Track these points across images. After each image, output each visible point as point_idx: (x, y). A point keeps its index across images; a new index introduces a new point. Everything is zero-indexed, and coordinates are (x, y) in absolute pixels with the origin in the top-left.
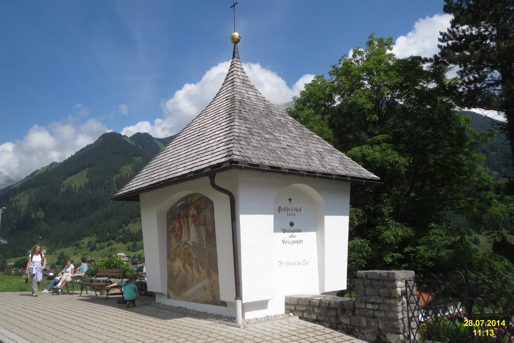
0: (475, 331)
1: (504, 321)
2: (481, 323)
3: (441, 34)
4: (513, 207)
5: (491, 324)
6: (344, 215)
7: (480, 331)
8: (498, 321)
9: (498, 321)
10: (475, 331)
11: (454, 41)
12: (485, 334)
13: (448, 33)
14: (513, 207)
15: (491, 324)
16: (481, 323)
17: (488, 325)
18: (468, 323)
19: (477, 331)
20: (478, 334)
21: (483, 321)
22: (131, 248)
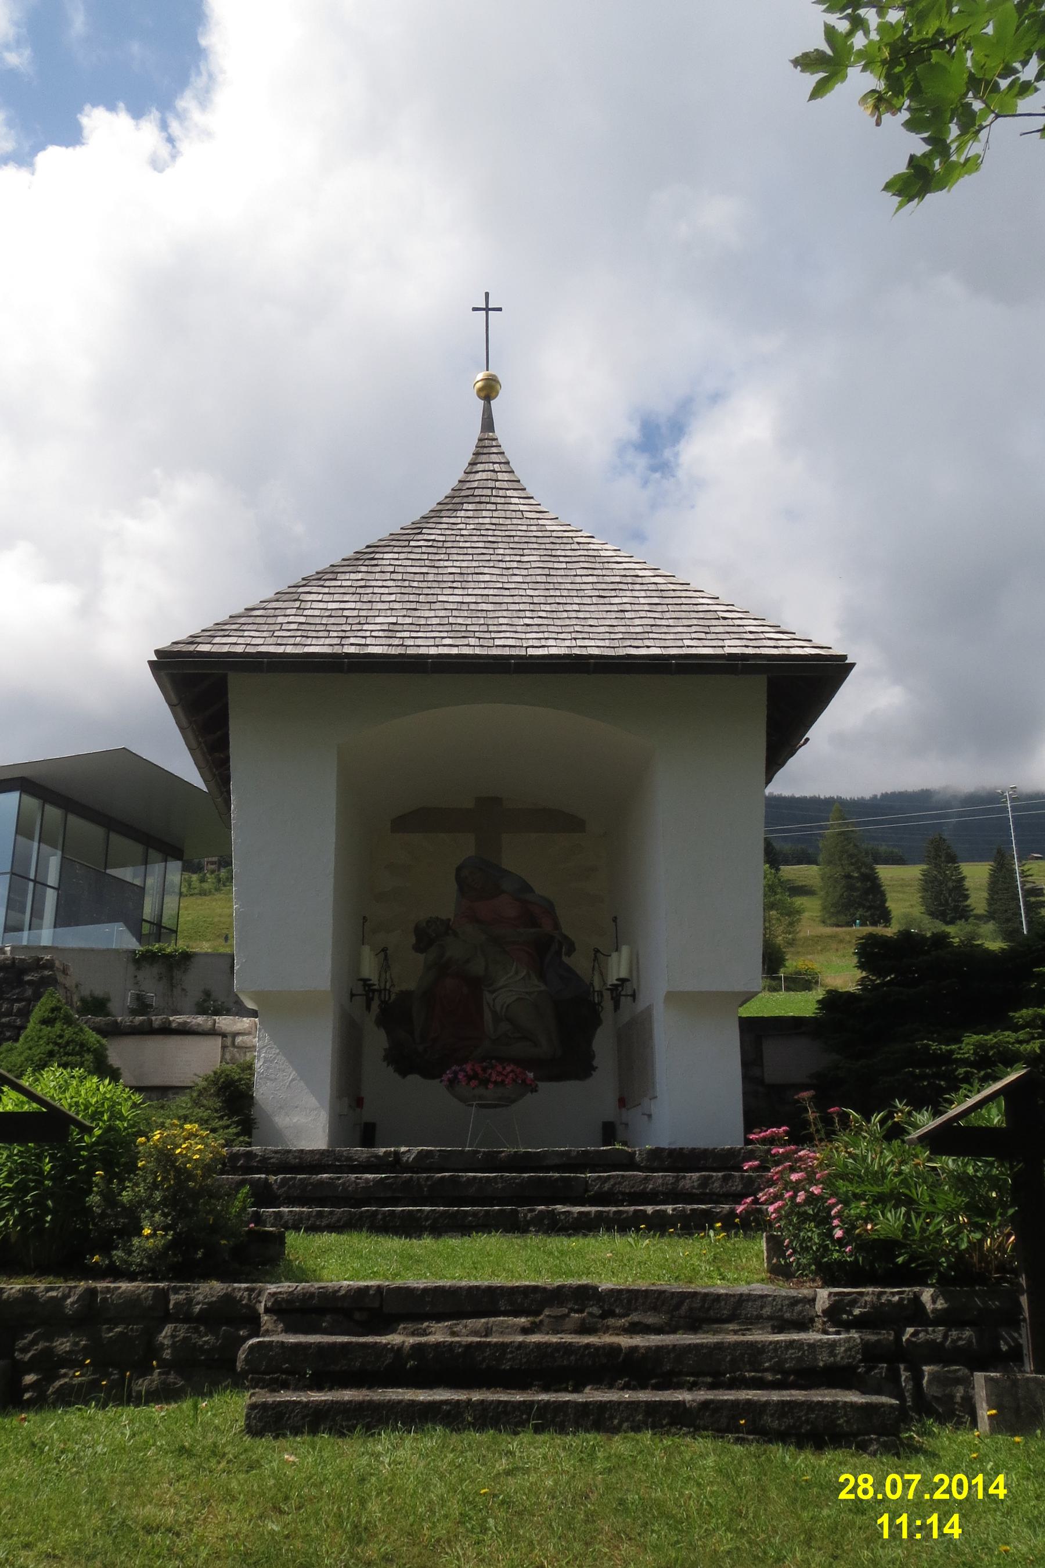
0: (885, 1519)
1: (1001, 1479)
2: (907, 1484)
3: (853, 665)
4: (1038, 1542)
5: (948, 1491)
6: (45, 893)
7: (904, 1519)
8: (979, 1479)
9: (979, 1479)
10: (885, 1519)
11: (1017, 1015)
12: (926, 1528)
13: (967, 903)
14: (1038, 1542)
15: (948, 1491)
16: (907, 1484)
17: (938, 1495)
18: (856, 1486)
19: (891, 1521)
20: (895, 1529)
21: (917, 1477)
22: (184, 890)
